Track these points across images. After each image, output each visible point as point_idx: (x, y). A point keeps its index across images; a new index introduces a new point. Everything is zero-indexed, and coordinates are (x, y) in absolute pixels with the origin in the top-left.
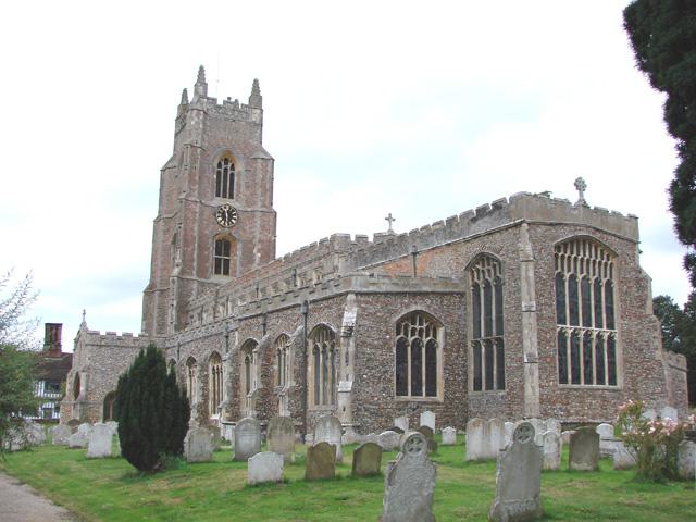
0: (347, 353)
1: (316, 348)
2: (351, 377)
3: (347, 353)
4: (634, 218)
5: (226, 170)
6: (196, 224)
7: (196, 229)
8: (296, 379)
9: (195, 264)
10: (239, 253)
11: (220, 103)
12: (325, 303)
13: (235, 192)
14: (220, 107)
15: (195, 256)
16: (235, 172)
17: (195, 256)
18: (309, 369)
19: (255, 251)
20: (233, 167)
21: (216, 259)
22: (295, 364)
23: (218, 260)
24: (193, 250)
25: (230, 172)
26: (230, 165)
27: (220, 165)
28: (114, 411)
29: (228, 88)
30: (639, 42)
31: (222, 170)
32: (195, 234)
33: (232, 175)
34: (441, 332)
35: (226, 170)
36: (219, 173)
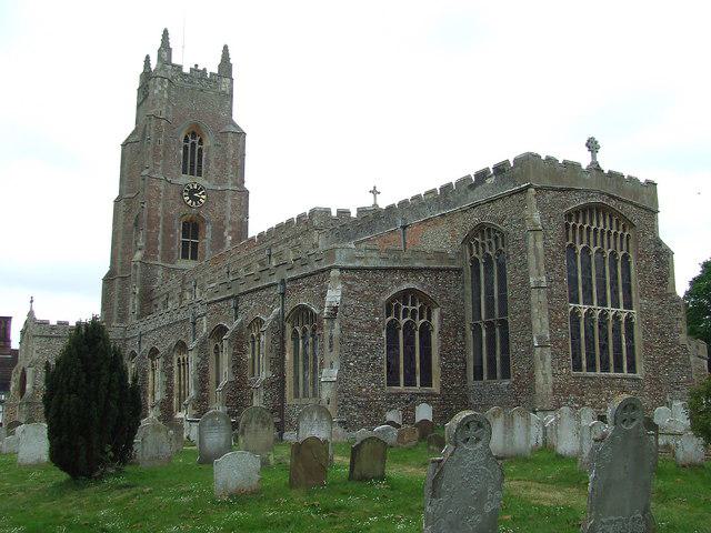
1: (295, 333)
5: (193, 144)
9: (159, 248)
10: (209, 236)
11: (186, 70)
12: (306, 280)
16: (204, 147)
18: (287, 357)
19: (226, 234)
20: (201, 142)
23: (185, 244)
25: (198, 147)
27: (186, 139)
29: (195, 54)
32: (159, 215)
33: (200, 150)
34: (436, 314)
35: (193, 144)
36: (186, 148)
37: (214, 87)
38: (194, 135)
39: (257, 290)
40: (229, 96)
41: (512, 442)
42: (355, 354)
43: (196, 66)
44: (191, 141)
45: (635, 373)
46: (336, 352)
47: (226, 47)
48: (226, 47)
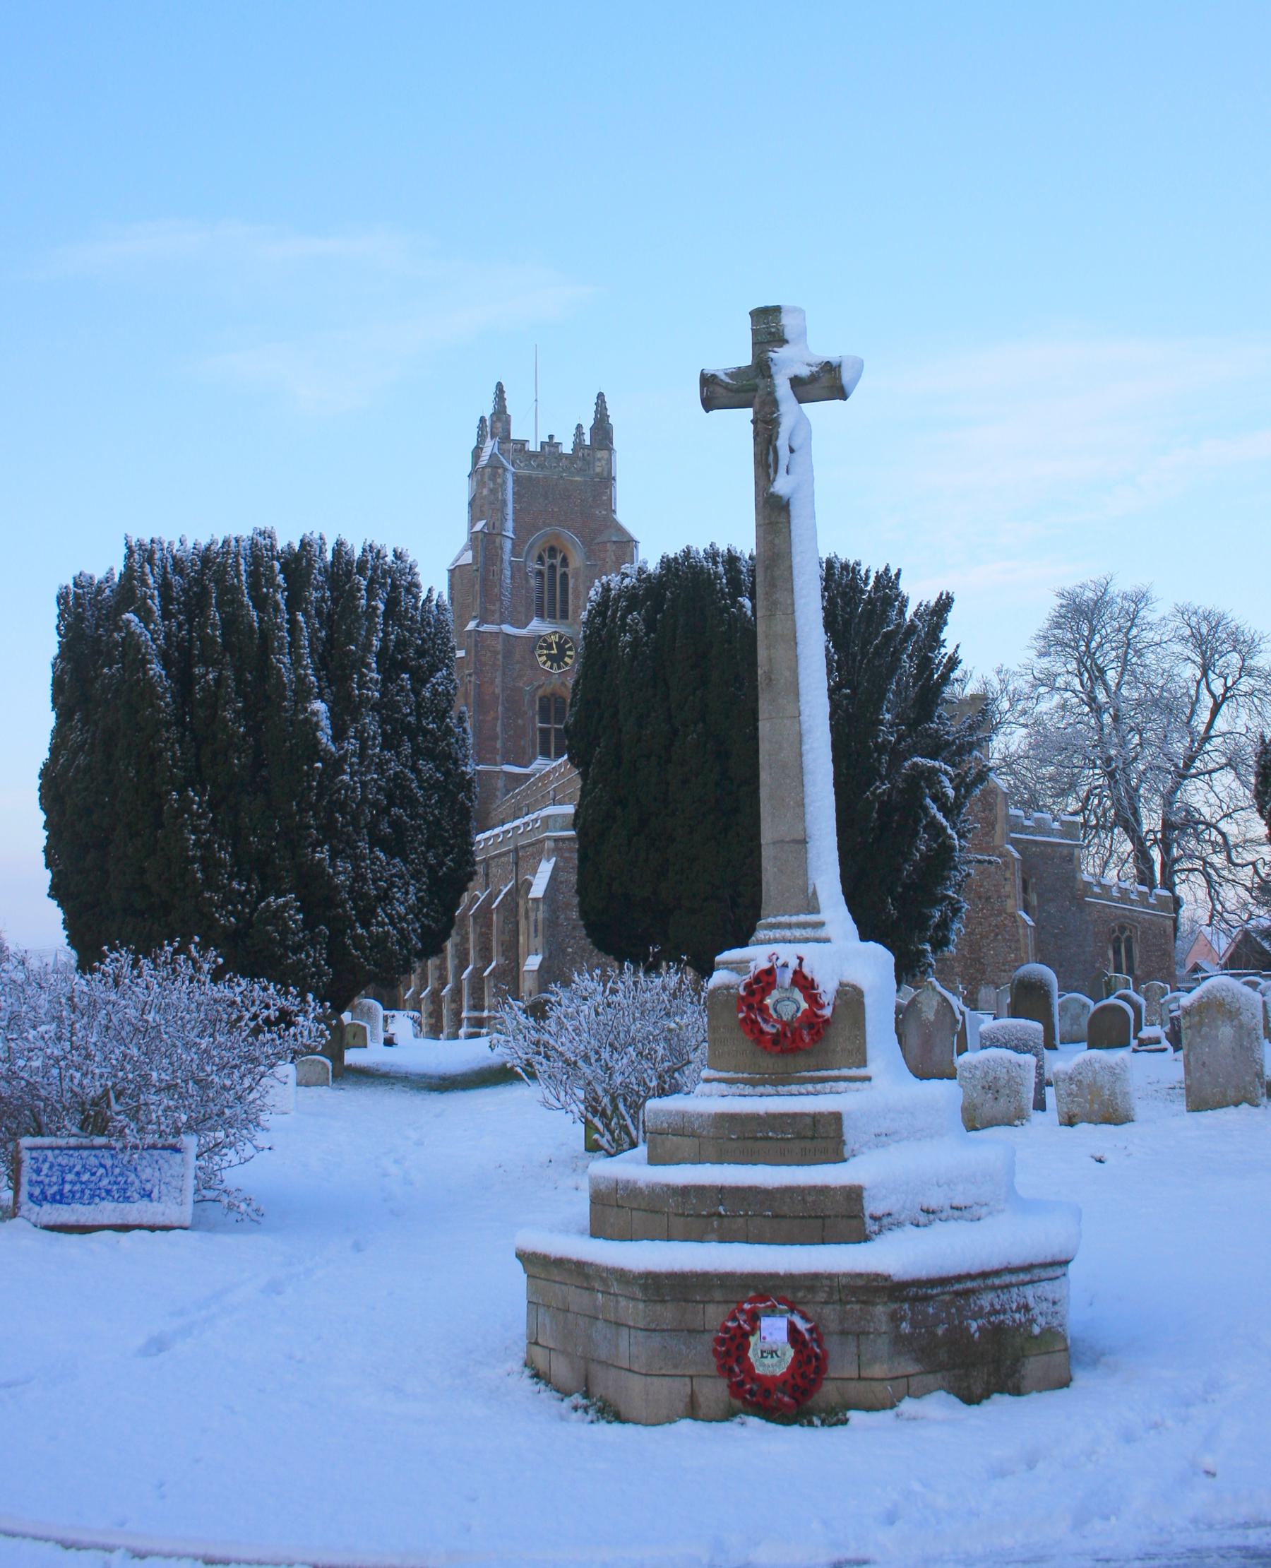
0: (536, 921)
2: (540, 950)
3: (536, 921)
4: (49, 895)
5: (552, 567)
6: (499, 673)
7: (498, 681)
8: (504, 953)
9: (499, 744)
13: (571, 608)
14: (534, 455)
15: (498, 729)
16: (569, 570)
17: (498, 729)
18: (521, 939)
20: (565, 562)
21: (541, 730)
22: (503, 933)
24: (497, 719)
25: (559, 571)
26: (559, 558)
28: (1023, 1028)
29: (548, 421)
30: (41, 804)
31: (545, 569)
32: (497, 691)
33: (564, 576)
35: (552, 567)
37: (707, 381)
38: (553, 551)
39: (500, 855)
40: (607, 480)
41: (1250, 806)
42: (574, 938)
43: (551, 437)
44: (548, 561)
45: (818, 912)
46: (540, 938)
47: (601, 396)
48: (601, 396)
